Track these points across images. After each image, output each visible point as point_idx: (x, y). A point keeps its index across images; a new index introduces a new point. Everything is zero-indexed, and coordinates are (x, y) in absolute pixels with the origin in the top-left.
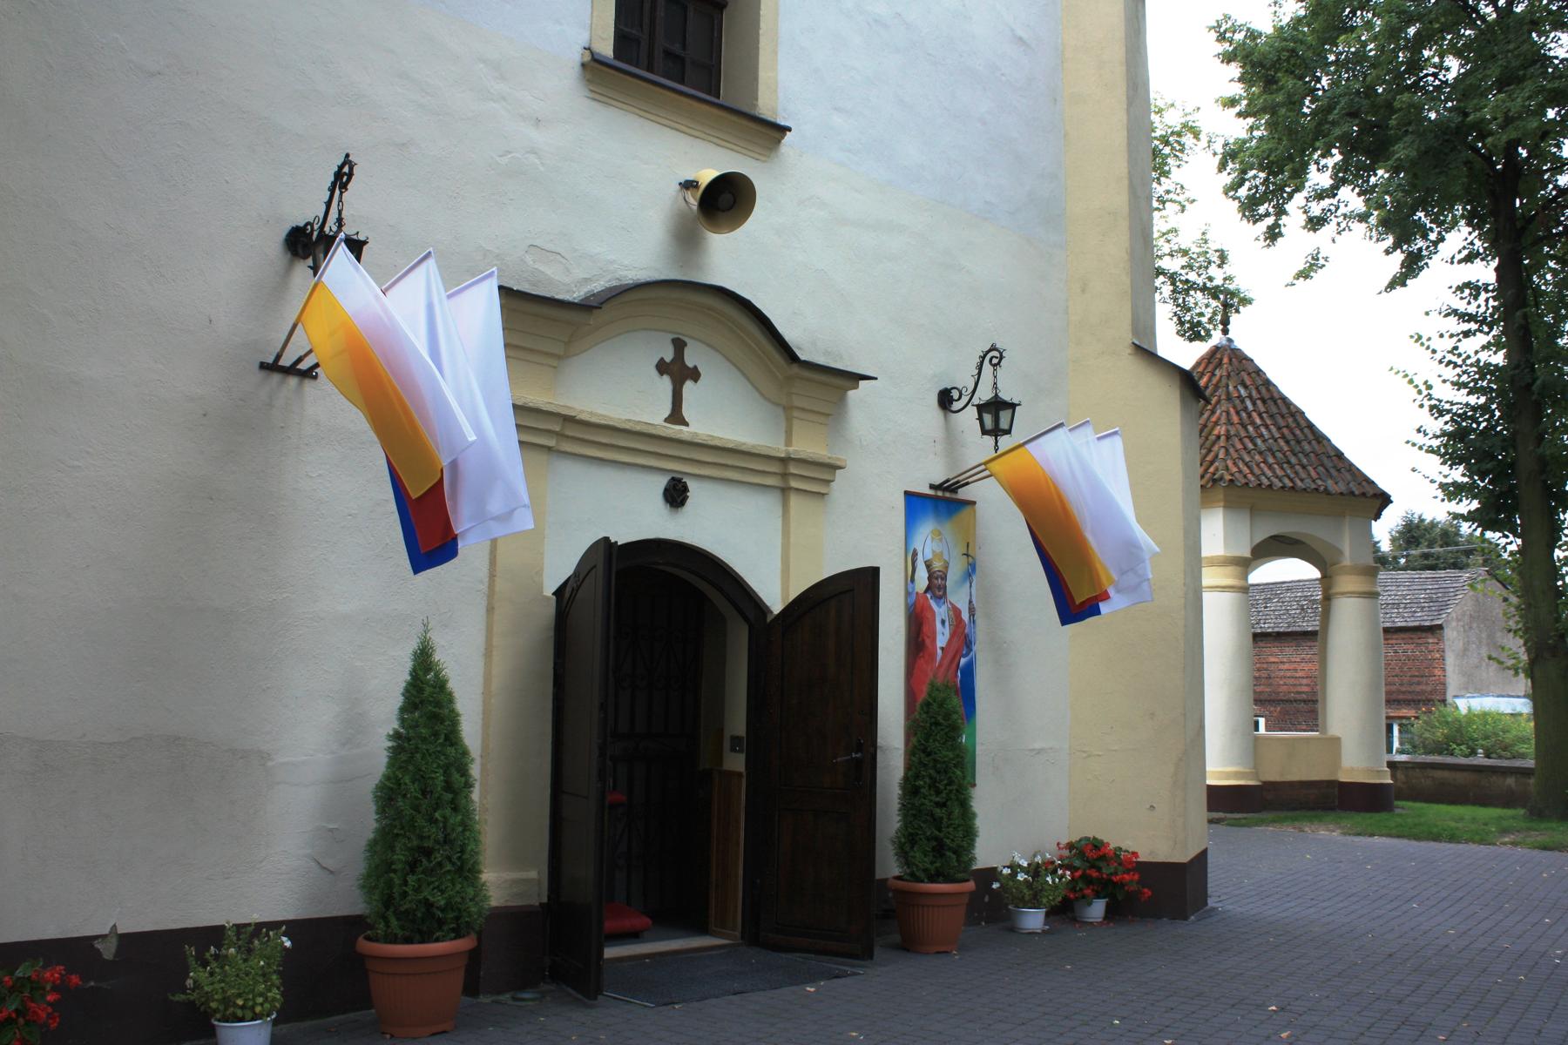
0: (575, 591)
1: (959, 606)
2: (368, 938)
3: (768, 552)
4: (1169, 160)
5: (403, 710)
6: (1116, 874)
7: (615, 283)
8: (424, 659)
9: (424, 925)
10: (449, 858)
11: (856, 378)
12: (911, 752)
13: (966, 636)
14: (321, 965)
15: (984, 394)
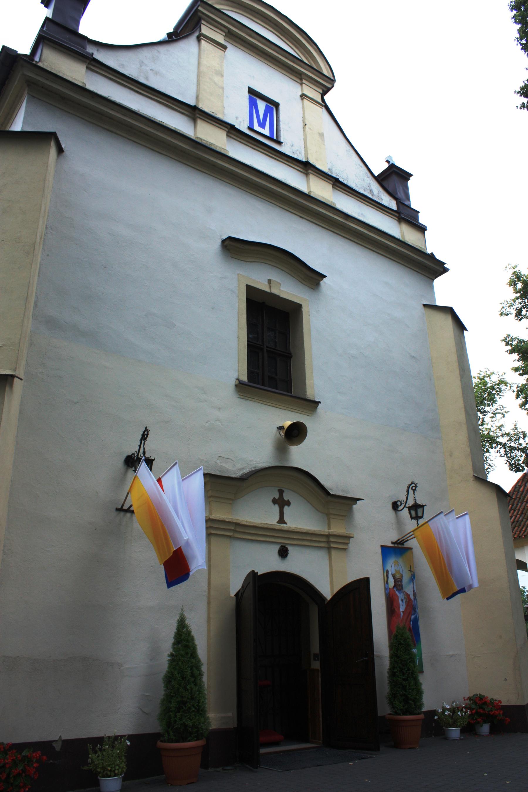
0: (243, 594)
1: (409, 593)
2: (162, 741)
3: (323, 574)
5: (174, 644)
6: (491, 711)
8: (182, 624)
9: (183, 734)
10: (193, 705)
11: (355, 500)
12: (391, 657)
13: (413, 606)
14: (142, 754)
15: (411, 502)
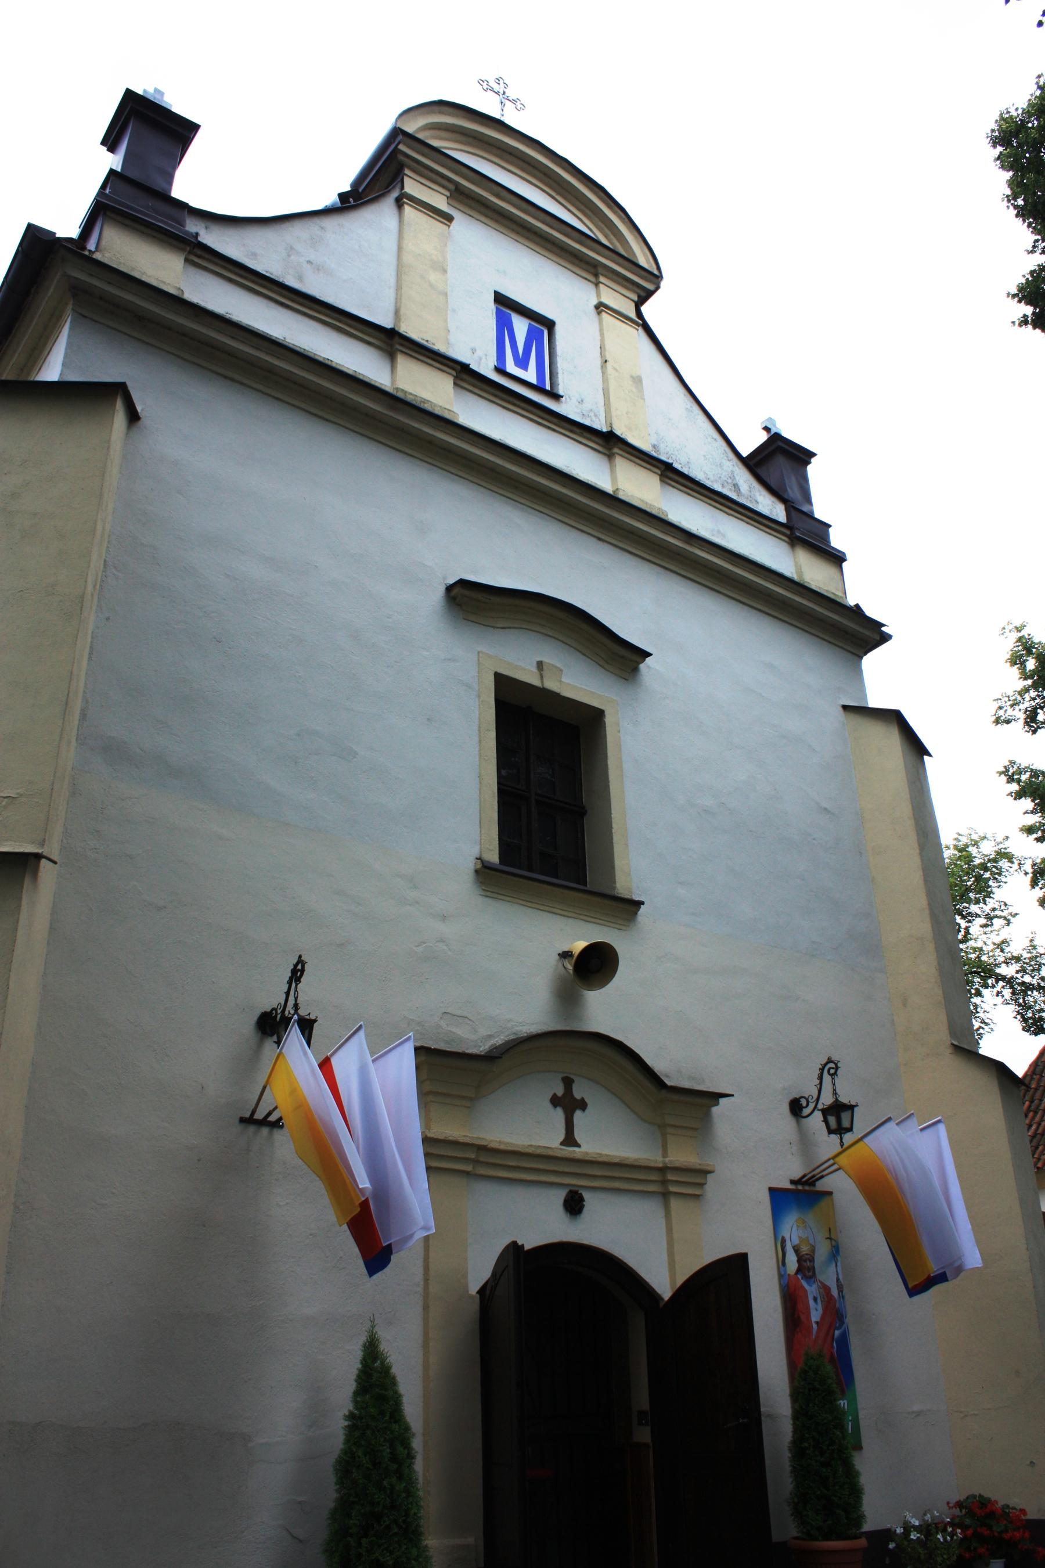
1: (828, 1284)
3: (652, 1247)
4: (991, 883)
5: (356, 1393)
7: (512, 1037)
8: (372, 1351)
11: (716, 1097)
15: (827, 1100)
